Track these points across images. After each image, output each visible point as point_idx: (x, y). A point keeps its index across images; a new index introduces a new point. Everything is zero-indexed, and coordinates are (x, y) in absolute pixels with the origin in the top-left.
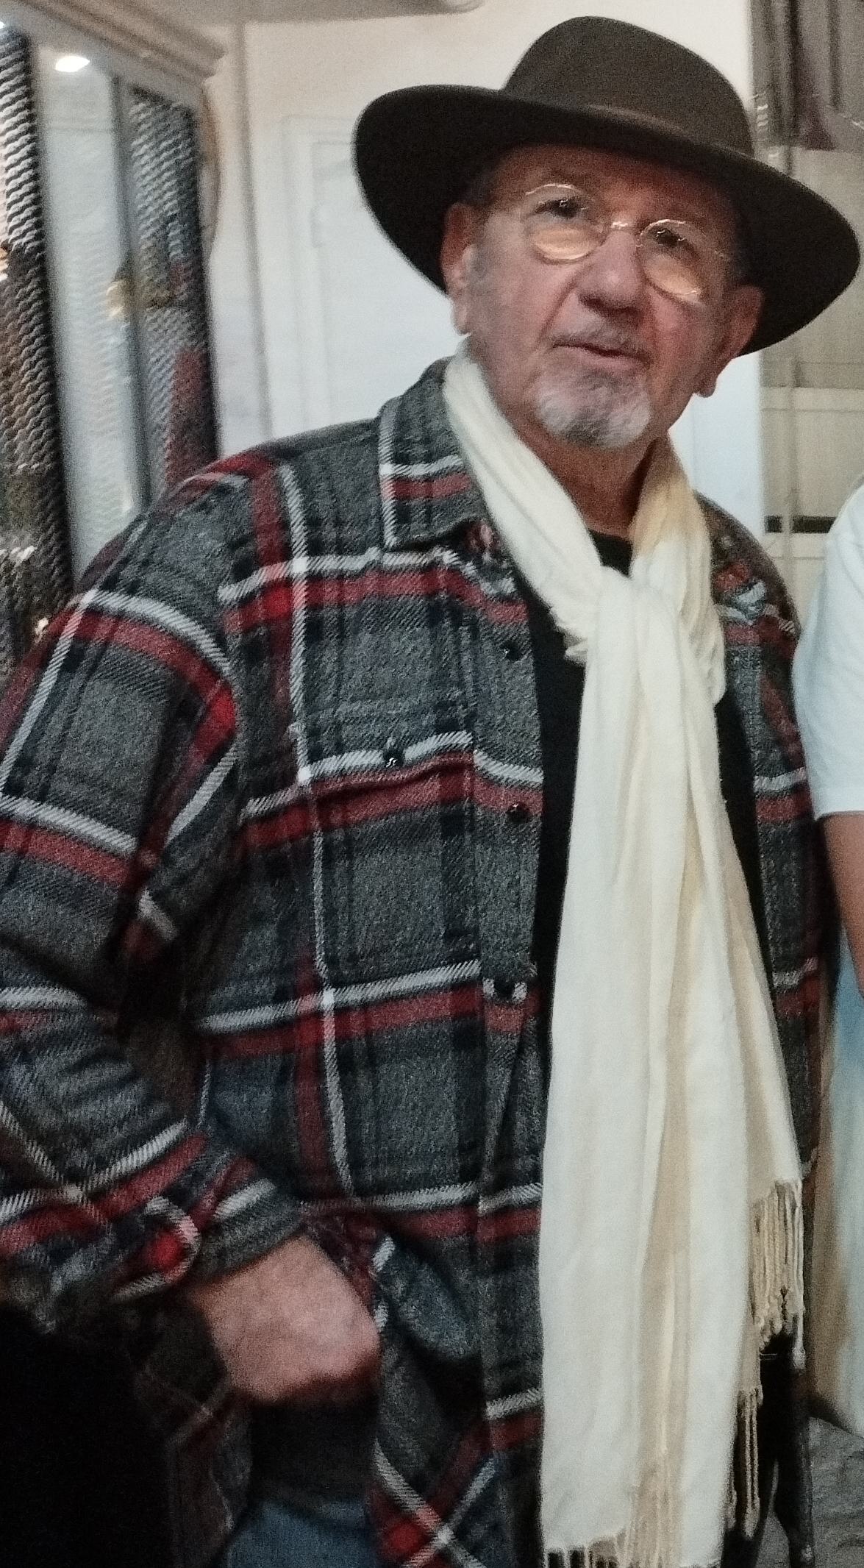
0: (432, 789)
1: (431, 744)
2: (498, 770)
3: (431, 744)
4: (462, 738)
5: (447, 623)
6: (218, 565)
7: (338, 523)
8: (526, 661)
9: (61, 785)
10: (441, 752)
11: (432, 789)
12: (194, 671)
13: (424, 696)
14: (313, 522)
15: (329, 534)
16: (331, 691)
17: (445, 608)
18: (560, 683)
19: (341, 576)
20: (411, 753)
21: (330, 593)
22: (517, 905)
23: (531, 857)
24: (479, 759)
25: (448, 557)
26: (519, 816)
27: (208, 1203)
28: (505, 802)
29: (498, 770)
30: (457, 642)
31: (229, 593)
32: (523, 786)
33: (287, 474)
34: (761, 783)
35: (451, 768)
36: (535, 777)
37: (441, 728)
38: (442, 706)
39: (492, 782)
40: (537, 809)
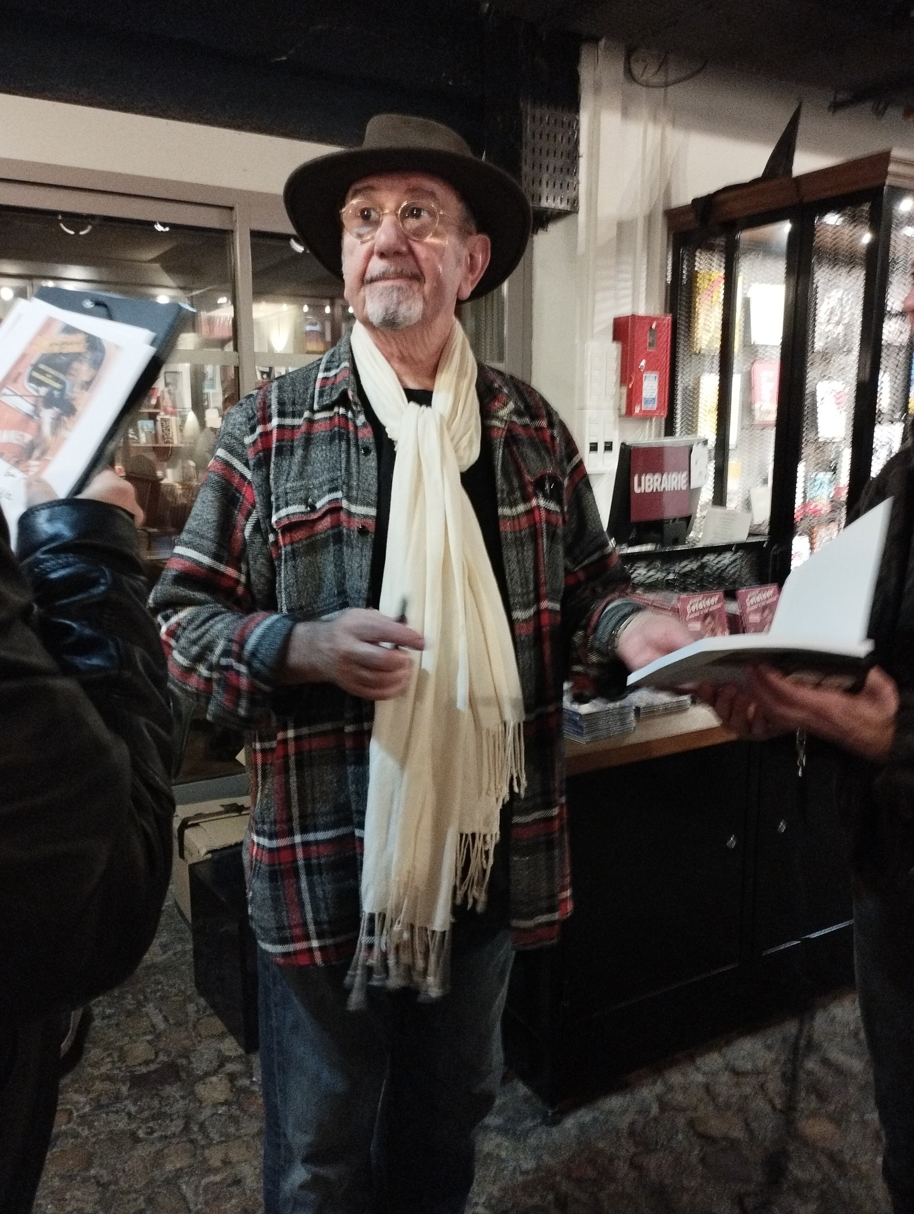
0: (327, 522)
1: (327, 498)
2: (356, 509)
3: (327, 498)
4: (339, 494)
5: (337, 441)
6: (244, 428)
7: (294, 404)
8: (373, 454)
9: (321, 821)
10: (330, 502)
11: (327, 522)
12: (236, 480)
13: (326, 476)
14: (281, 403)
15: (289, 409)
16: (284, 478)
17: (341, 434)
18: (385, 450)
19: (293, 427)
20: (318, 505)
21: (287, 435)
22: (361, 576)
23: (368, 553)
24: (345, 504)
25: (342, 411)
26: (363, 531)
27: (321, 850)
28: (356, 524)
29: (356, 509)
30: (340, 446)
31: (248, 440)
32: (366, 516)
33: (517, 819)
34: (504, 511)
35: (334, 510)
36: (372, 512)
37: (332, 490)
38: (332, 480)
39: (350, 514)
40: (372, 528)
